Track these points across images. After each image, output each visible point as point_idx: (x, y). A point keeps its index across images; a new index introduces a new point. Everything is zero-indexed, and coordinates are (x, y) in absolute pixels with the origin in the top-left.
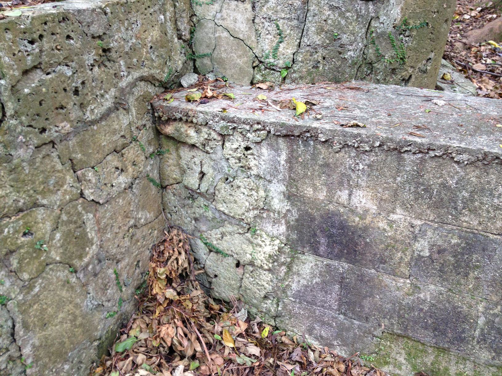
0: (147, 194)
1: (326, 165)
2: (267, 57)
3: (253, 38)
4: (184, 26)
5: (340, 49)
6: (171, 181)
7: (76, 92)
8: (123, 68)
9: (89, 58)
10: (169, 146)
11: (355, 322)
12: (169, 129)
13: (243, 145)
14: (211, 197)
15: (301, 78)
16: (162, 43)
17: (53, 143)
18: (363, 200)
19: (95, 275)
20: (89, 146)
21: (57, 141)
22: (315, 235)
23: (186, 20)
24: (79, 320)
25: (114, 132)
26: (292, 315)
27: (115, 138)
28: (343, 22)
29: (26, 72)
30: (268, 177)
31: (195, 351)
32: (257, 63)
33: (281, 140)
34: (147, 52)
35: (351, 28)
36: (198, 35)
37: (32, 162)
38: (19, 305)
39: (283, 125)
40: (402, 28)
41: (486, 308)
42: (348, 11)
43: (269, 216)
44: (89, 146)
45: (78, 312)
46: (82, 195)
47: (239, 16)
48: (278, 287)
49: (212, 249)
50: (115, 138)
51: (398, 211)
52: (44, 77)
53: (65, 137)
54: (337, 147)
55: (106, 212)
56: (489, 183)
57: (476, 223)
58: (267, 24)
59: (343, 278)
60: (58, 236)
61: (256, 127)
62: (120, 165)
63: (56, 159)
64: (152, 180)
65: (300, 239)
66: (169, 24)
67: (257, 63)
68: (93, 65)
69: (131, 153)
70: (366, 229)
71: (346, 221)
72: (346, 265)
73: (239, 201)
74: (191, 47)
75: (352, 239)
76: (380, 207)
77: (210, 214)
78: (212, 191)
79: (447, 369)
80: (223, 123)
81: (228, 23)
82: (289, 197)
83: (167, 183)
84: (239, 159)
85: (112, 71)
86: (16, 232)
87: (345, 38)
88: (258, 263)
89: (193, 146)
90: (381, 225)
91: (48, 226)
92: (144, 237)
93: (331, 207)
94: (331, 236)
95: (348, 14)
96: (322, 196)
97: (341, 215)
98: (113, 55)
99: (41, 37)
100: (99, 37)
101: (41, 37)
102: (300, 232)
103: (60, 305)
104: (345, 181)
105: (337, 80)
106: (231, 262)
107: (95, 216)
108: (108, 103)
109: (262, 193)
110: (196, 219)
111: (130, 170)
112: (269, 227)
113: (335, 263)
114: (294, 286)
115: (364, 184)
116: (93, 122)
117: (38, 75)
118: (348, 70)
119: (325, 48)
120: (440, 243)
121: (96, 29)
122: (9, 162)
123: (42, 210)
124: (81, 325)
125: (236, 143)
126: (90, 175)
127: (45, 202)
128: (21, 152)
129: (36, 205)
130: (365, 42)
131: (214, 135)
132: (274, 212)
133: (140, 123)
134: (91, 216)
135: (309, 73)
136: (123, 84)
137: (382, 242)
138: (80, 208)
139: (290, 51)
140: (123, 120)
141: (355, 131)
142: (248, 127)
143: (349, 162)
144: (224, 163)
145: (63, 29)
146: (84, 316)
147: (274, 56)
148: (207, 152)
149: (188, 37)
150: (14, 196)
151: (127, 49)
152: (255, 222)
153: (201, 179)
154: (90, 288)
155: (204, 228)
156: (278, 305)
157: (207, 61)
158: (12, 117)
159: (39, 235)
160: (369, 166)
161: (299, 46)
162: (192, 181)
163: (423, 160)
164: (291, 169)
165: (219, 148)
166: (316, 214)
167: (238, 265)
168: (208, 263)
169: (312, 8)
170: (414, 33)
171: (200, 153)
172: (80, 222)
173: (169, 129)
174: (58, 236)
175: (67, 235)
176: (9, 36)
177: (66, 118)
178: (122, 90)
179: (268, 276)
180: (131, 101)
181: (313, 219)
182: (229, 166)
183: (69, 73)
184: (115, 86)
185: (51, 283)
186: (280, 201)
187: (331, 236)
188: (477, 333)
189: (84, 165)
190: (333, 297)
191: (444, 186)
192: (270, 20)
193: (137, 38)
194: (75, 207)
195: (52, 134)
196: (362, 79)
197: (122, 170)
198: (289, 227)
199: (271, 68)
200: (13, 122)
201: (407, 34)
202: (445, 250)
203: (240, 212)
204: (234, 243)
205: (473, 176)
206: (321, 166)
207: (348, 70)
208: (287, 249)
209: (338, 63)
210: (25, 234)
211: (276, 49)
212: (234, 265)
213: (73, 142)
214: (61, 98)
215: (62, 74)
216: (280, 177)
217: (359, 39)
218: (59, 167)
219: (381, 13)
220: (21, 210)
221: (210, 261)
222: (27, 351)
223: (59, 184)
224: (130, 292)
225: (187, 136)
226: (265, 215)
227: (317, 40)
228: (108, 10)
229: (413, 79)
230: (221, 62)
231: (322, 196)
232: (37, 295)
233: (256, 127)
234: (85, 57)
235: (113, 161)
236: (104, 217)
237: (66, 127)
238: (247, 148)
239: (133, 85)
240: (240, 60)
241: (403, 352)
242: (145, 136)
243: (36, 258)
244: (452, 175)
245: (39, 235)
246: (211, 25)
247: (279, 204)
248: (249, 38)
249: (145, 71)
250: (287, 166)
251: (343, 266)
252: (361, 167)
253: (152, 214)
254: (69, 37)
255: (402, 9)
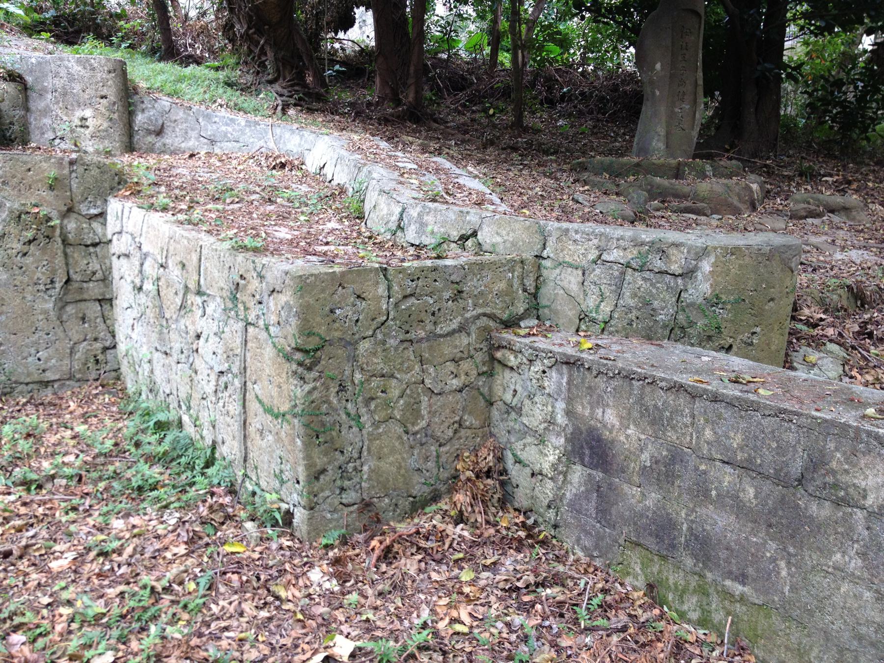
0: (476, 404)
1: (590, 388)
2: (591, 312)
3: (581, 296)
4: (530, 283)
5: (652, 312)
6: (497, 398)
7: (433, 314)
8: (470, 305)
9: (447, 295)
10: (498, 368)
11: (607, 530)
12: (499, 355)
13: (541, 368)
14: (519, 411)
15: (617, 332)
16: (509, 292)
17: (411, 341)
18: (611, 417)
19: (422, 445)
20: (435, 351)
21: (415, 341)
22: (582, 447)
23: (532, 279)
24: (403, 471)
25: (456, 347)
26: (567, 525)
27: (455, 351)
28: (654, 291)
29: (405, 297)
30: (556, 396)
31: (476, 520)
32: (583, 316)
33: (564, 367)
34: (492, 297)
35: (662, 296)
36: (543, 291)
37: (396, 349)
38: (368, 434)
39: (565, 354)
40: (714, 301)
41: (687, 515)
42: (658, 282)
43: (554, 429)
44: (435, 351)
45: (403, 464)
46: (423, 382)
47: (573, 279)
48: (557, 495)
49: (518, 461)
50: (455, 351)
51: (631, 426)
52: (416, 301)
53: (420, 341)
54: (595, 373)
55: (438, 401)
56: (680, 405)
57: (675, 438)
58: (592, 287)
59: (599, 487)
60: (402, 402)
61: (550, 355)
62: (455, 371)
63: (411, 353)
64: (482, 394)
65: (573, 451)
66: (516, 280)
67: (583, 316)
68: (448, 300)
69: (465, 365)
70: (612, 442)
71: (601, 434)
72: (601, 474)
73: (535, 416)
74: (536, 299)
75: (604, 451)
76: (621, 423)
77: (517, 427)
78: (519, 405)
79: (667, 579)
80: (530, 351)
81: (565, 284)
82: (569, 413)
83: (493, 400)
84: (538, 380)
85: (461, 306)
86: (378, 387)
87: (656, 304)
88: (544, 472)
89: (512, 368)
90: (621, 438)
91: (397, 393)
92: (467, 438)
93: (592, 422)
94: (590, 448)
95: (658, 285)
96: (587, 413)
97: (597, 429)
98: (464, 295)
99: (418, 278)
100: (457, 283)
101: (418, 278)
102: (573, 445)
103: (393, 451)
104: (599, 402)
105: (649, 337)
106: (528, 471)
107: (429, 400)
108: (454, 325)
109: (550, 408)
110: (509, 432)
111: (463, 377)
112: (553, 439)
113: (594, 472)
114: (568, 495)
115: (611, 404)
116: (441, 336)
117: (413, 300)
118: (660, 331)
119: (639, 310)
120: (656, 455)
121: (454, 278)
122: (384, 345)
123: (395, 381)
124: (403, 476)
125: (538, 367)
126: (432, 370)
127: (398, 376)
128: (392, 341)
129: (392, 376)
130: (675, 308)
131: (525, 360)
132: (557, 425)
133: (478, 346)
134: (426, 399)
135: (624, 329)
136: (468, 315)
137: (623, 454)
138: (420, 391)
139: (608, 309)
140: (463, 340)
141: (605, 362)
142: (544, 355)
143: (603, 386)
144: (529, 383)
145: (434, 275)
146: (407, 471)
147: (596, 312)
148: (520, 374)
149: (533, 291)
150: (382, 365)
151: (476, 293)
152: (545, 433)
153: (514, 396)
154: (416, 452)
155: (513, 440)
156: (557, 515)
157: (546, 311)
158: (392, 320)
159: (390, 395)
160: (614, 389)
161: (616, 305)
162: (508, 397)
163: (643, 386)
164: (569, 390)
165: (527, 370)
166: (583, 428)
167: (533, 475)
168: (513, 473)
169: (627, 278)
170: (729, 307)
171: (516, 375)
172: (418, 400)
173: (499, 355)
174: (402, 402)
175: (407, 404)
176: (401, 276)
177: (423, 328)
178: (467, 319)
179: (550, 484)
180: (473, 328)
181: (581, 433)
182: (532, 386)
183: (432, 302)
184: (462, 316)
185: (390, 432)
186: (562, 416)
187: (590, 448)
188: (683, 539)
189: (429, 362)
190: (591, 507)
191: (655, 406)
192: (595, 284)
193: (485, 286)
194: (417, 388)
195: (412, 336)
196: (675, 341)
197: (456, 376)
198: (567, 440)
199: (593, 321)
200: (392, 323)
201: (720, 306)
202: (659, 461)
203: (535, 425)
204: (530, 454)
205: (671, 398)
206: (587, 388)
207: (660, 331)
208: (564, 459)
209: (651, 324)
210: (382, 392)
211: (598, 306)
212: (530, 475)
213: (424, 345)
214: (423, 316)
215: (426, 302)
216: (563, 396)
217: (669, 306)
218: (412, 358)
219: (689, 286)
220: (383, 376)
221: (514, 471)
222: (365, 468)
223: (410, 369)
224: (446, 475)
225: (509, 360)
226: (551, 428)
227: (632, 302)
228: (466, 267)
229: (735, 348)
230: (556, 312)
231: (587, 413)
232: (380, 434)
233: (550, 355)
234: (444, 294)
235: (451, 366)
236: (435, 404)
237: (422, 334)
238: (544, 372)
239: (478, 317)
240: (570, 313)
241: (639, 561)
242: (479, 357)
243: (385, 409)
244: (660, 398)
245: (390, 395)
246: (552, 284)
247: (561, 419)
248: (578, 296)
249: (488, 310)
250: (567, 387)
251: (598, 475)
252: (609, 389)
253: (478, 422)
254: (435, 281)
255: (711, 285)
